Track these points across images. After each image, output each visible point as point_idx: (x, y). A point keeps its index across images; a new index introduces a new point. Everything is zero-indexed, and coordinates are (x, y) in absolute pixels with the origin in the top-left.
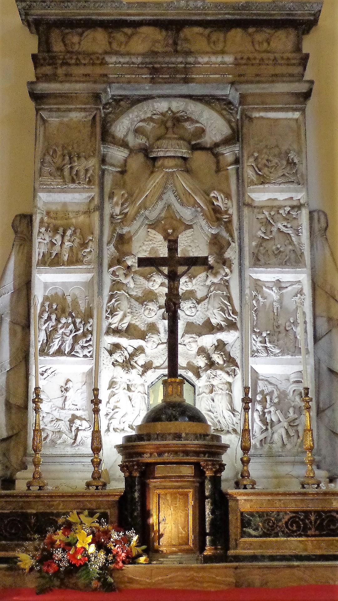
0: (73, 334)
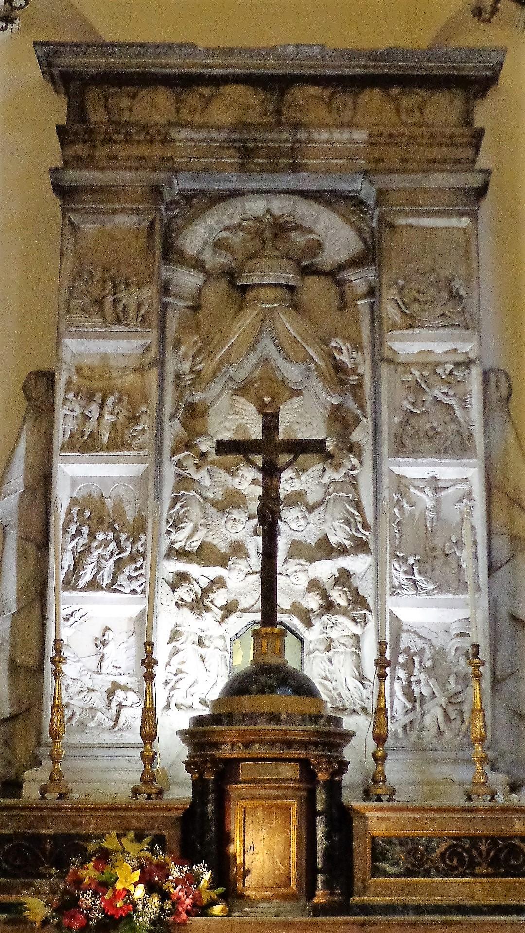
0: (115, 558)
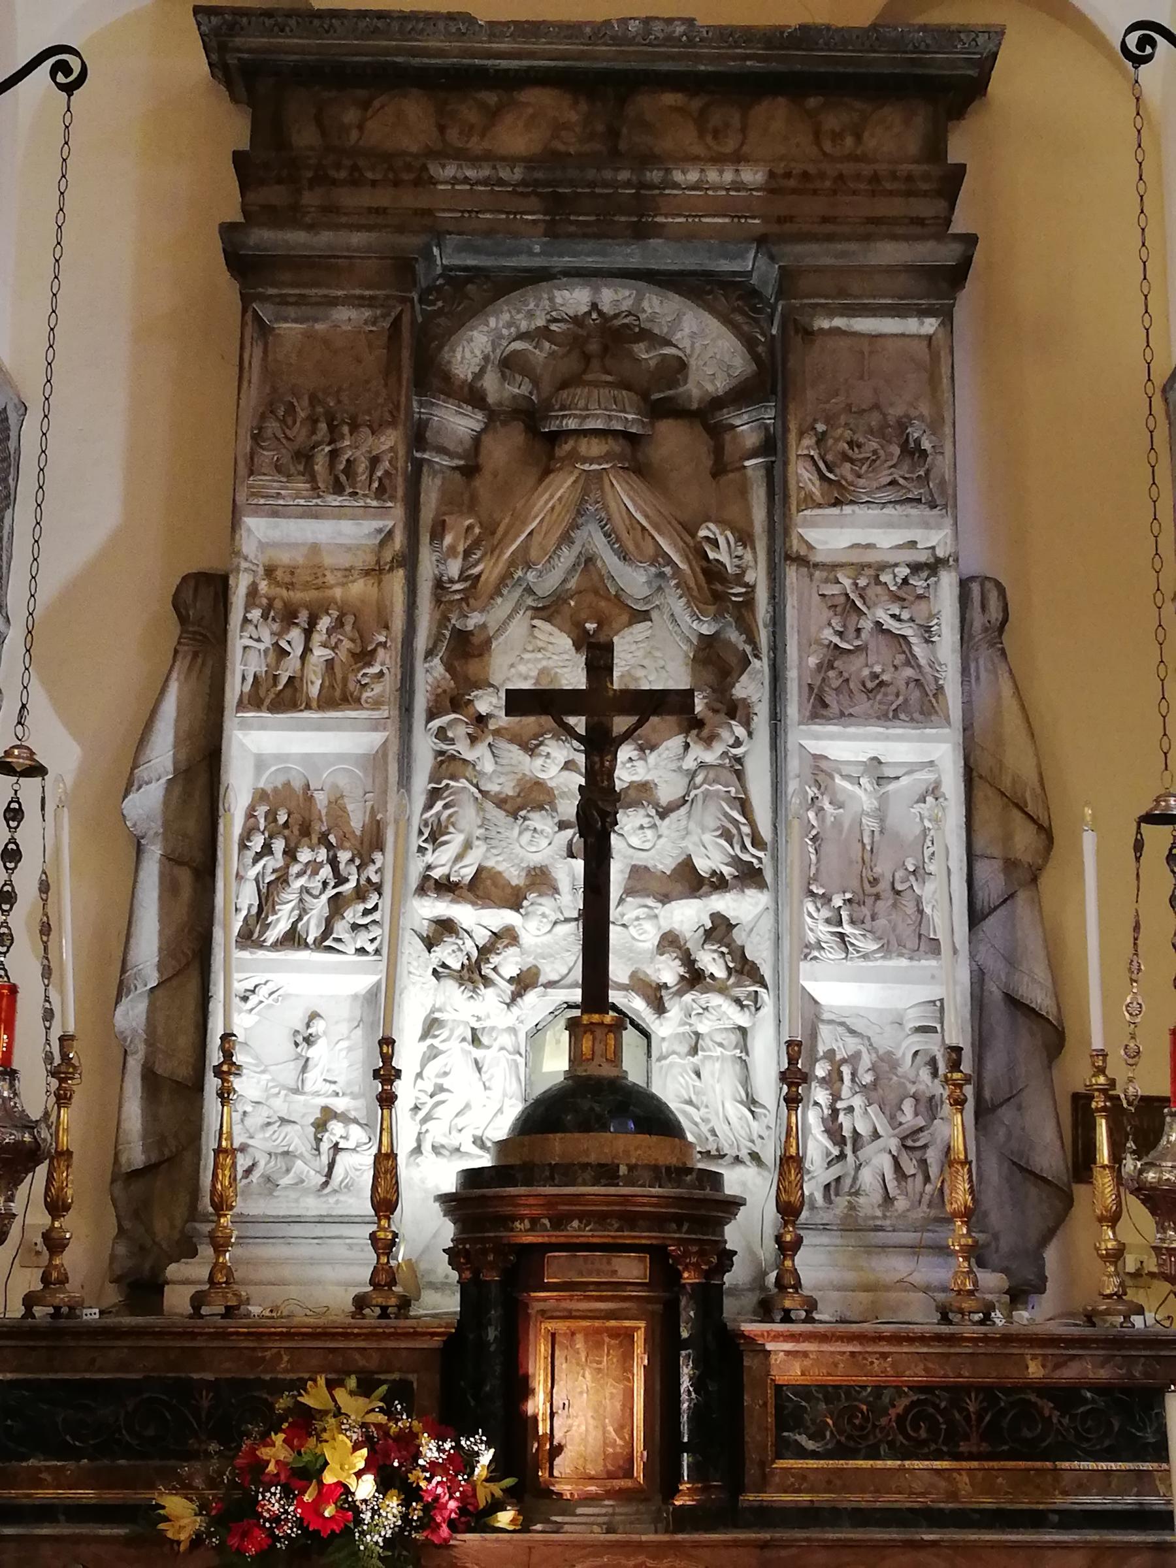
0: (330, 892)
